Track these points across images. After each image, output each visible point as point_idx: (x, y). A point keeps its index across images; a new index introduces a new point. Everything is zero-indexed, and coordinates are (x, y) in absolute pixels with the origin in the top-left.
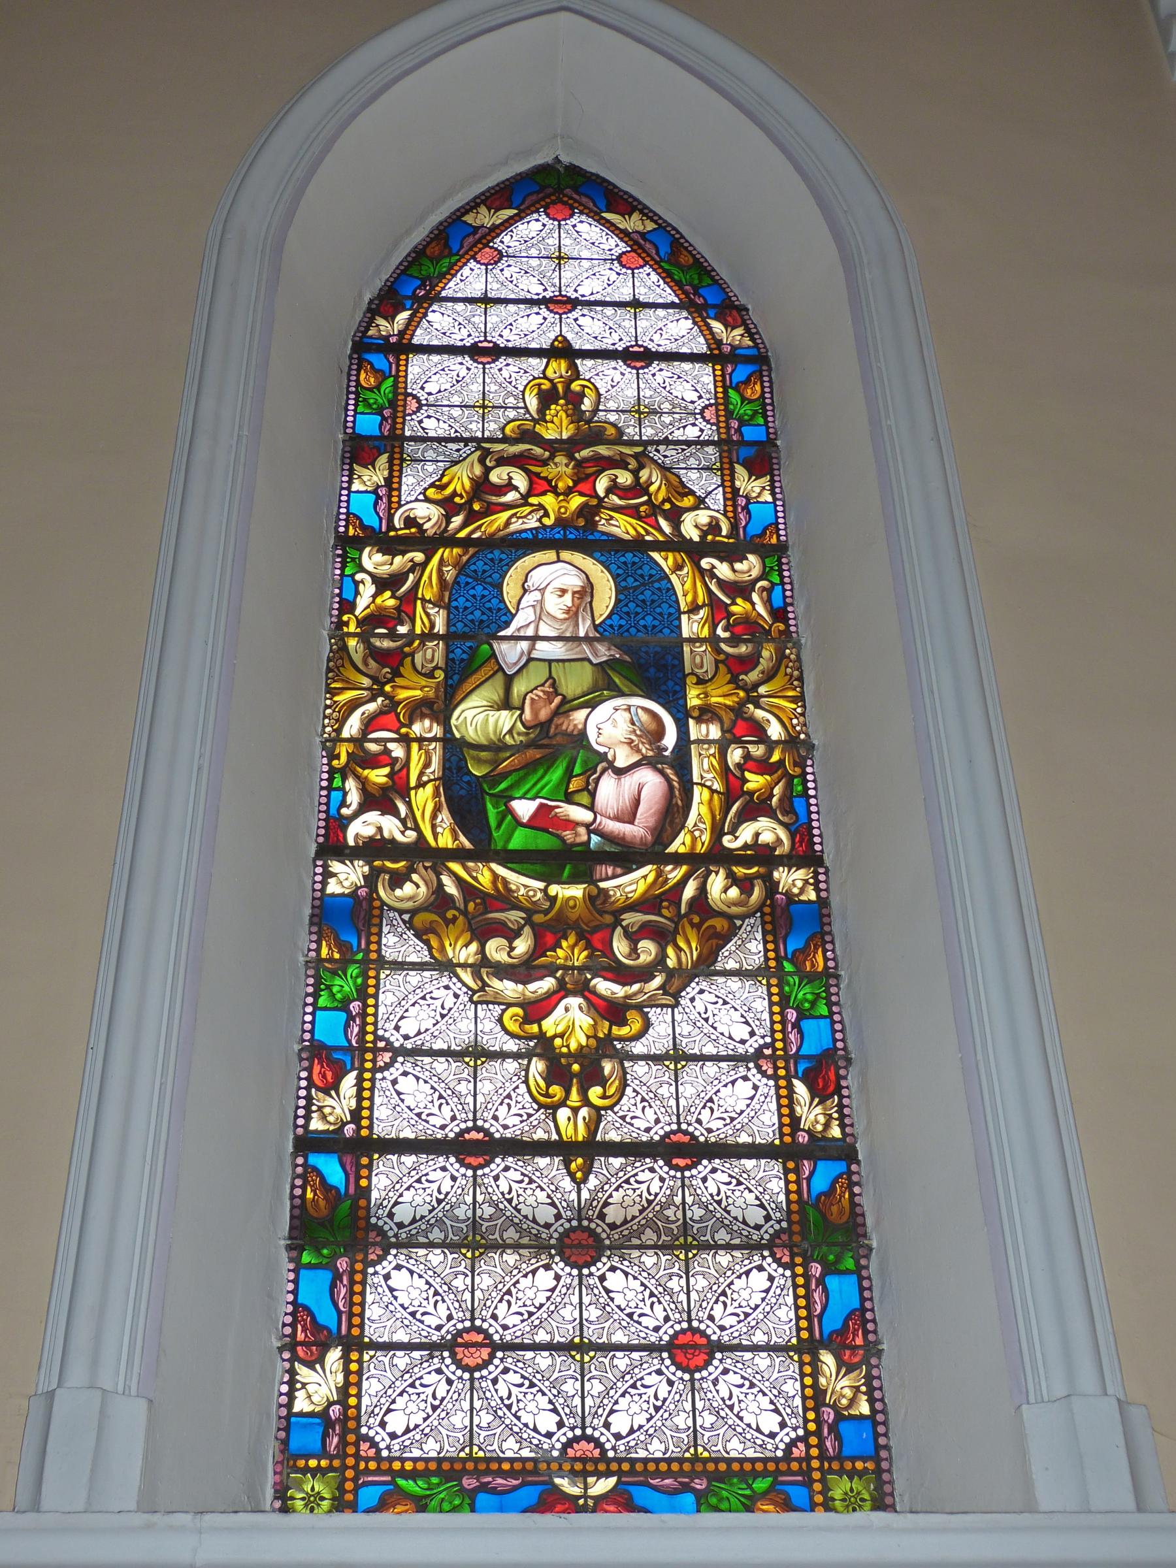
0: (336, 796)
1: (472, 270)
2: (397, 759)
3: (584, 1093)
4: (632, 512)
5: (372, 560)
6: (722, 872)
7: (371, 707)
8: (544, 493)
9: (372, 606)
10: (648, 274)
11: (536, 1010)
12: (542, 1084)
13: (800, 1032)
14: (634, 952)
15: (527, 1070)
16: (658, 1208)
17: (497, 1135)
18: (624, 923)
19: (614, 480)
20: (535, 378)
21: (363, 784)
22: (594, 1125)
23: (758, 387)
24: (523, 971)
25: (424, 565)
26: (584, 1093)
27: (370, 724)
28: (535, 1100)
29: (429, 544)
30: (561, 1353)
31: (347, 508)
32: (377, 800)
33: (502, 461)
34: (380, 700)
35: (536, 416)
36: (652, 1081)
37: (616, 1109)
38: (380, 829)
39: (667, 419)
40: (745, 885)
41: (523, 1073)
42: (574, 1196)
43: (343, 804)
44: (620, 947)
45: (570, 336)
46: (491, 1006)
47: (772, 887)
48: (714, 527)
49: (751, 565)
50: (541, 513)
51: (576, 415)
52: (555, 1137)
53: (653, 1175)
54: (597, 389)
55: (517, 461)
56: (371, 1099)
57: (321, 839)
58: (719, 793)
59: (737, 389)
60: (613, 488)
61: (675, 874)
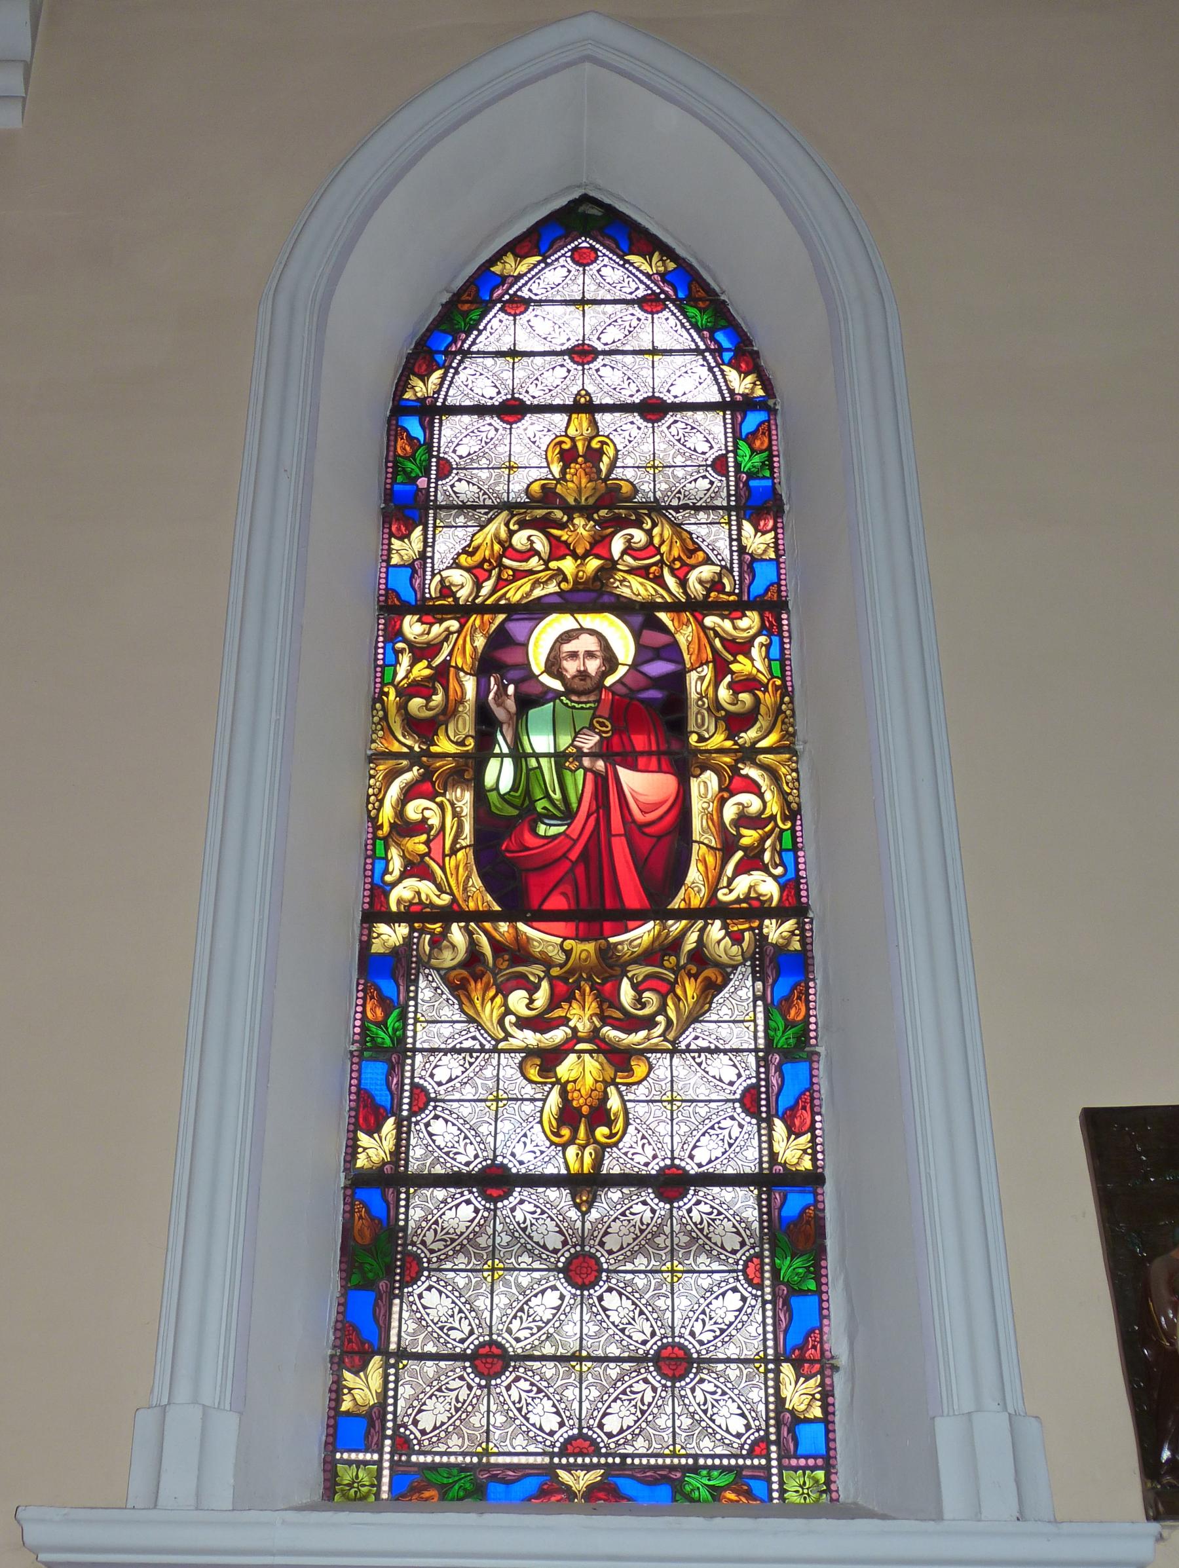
0: (380, 866)
1: (501, 321)
2: (431, 827)
3: (591, 1131)
4: (643, 572)
5: (412, 627)
6: (718, 923)
7: (408, 777)
8: (563, 557)
9: (412, 676)
10: (667, 319)
11: (549, 1059)
12: (554, 1123)
13: (782, 1076)
14: (640, 1003)
15: (541, 1112)
16: (649, 1236)
17: (514, 1171)
18: (630, 975)
19: (629, 539)
20: (557, 436)
21: (403, 851)
22: (598, 1162)
23: (766, 440)
24: (539, 1023)
25: (459, 632)
26: (591, 1131)
27: (409, 793)
28: (548, 1138)
29: (462, 612)
30: (563, 1365)
31: (386, 584)
32: (416, 868)
33: (523, 525)
34: (415, 768)
35: (557, 476)
36: (651, 1119)
37: (620, 1145)
38: (418, 893)
39: (680, 473)
40: (737, 939)
41: (538, 1114)
42: (579, 1224)
43: (386, 871)
44: (626, 994)
45: (590, 388)
46: (513, 1055)
47: (762, 939)
48: (715, 585)
49: (750, 621)
50: (560, 578)
51: (593, 472)
52: (563, 1171)
53: (645, 1207)
54: (615, 445)
55: (542, 525)
56: (408, 1140)
57: (366, 906)
58: (719, 850)
59: (746, 440)
60: (628, 550)
61: (676, 927)
